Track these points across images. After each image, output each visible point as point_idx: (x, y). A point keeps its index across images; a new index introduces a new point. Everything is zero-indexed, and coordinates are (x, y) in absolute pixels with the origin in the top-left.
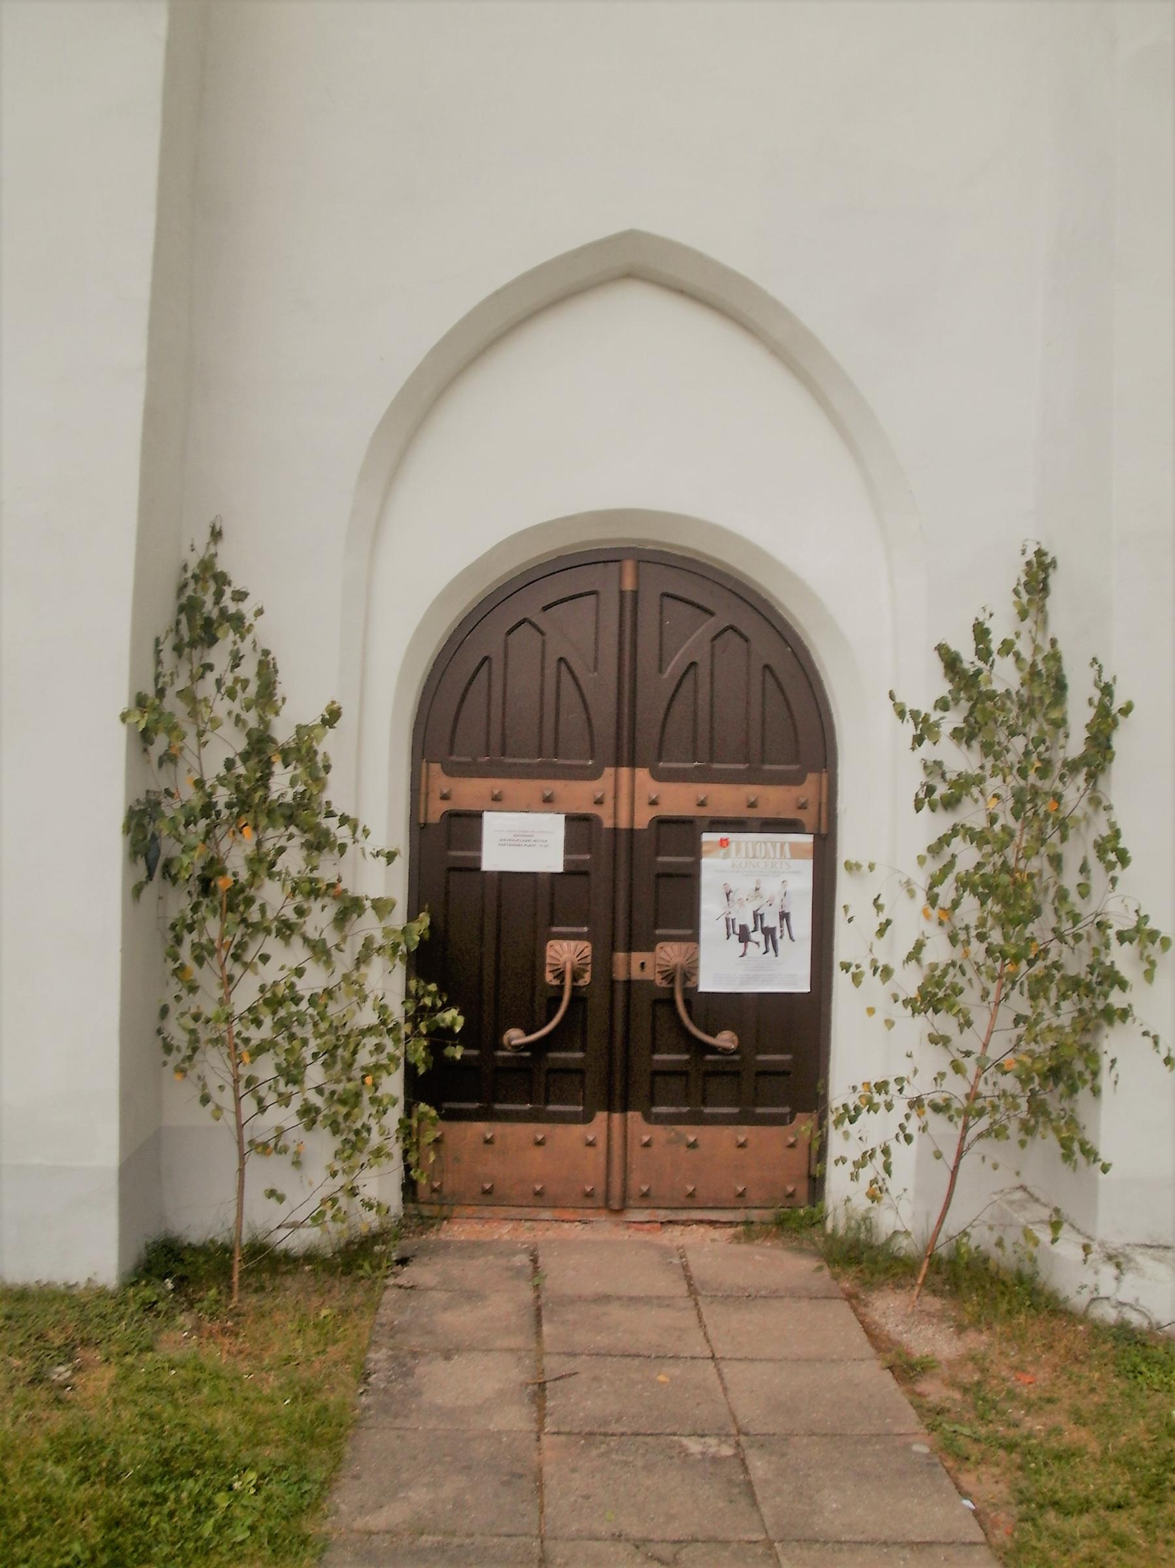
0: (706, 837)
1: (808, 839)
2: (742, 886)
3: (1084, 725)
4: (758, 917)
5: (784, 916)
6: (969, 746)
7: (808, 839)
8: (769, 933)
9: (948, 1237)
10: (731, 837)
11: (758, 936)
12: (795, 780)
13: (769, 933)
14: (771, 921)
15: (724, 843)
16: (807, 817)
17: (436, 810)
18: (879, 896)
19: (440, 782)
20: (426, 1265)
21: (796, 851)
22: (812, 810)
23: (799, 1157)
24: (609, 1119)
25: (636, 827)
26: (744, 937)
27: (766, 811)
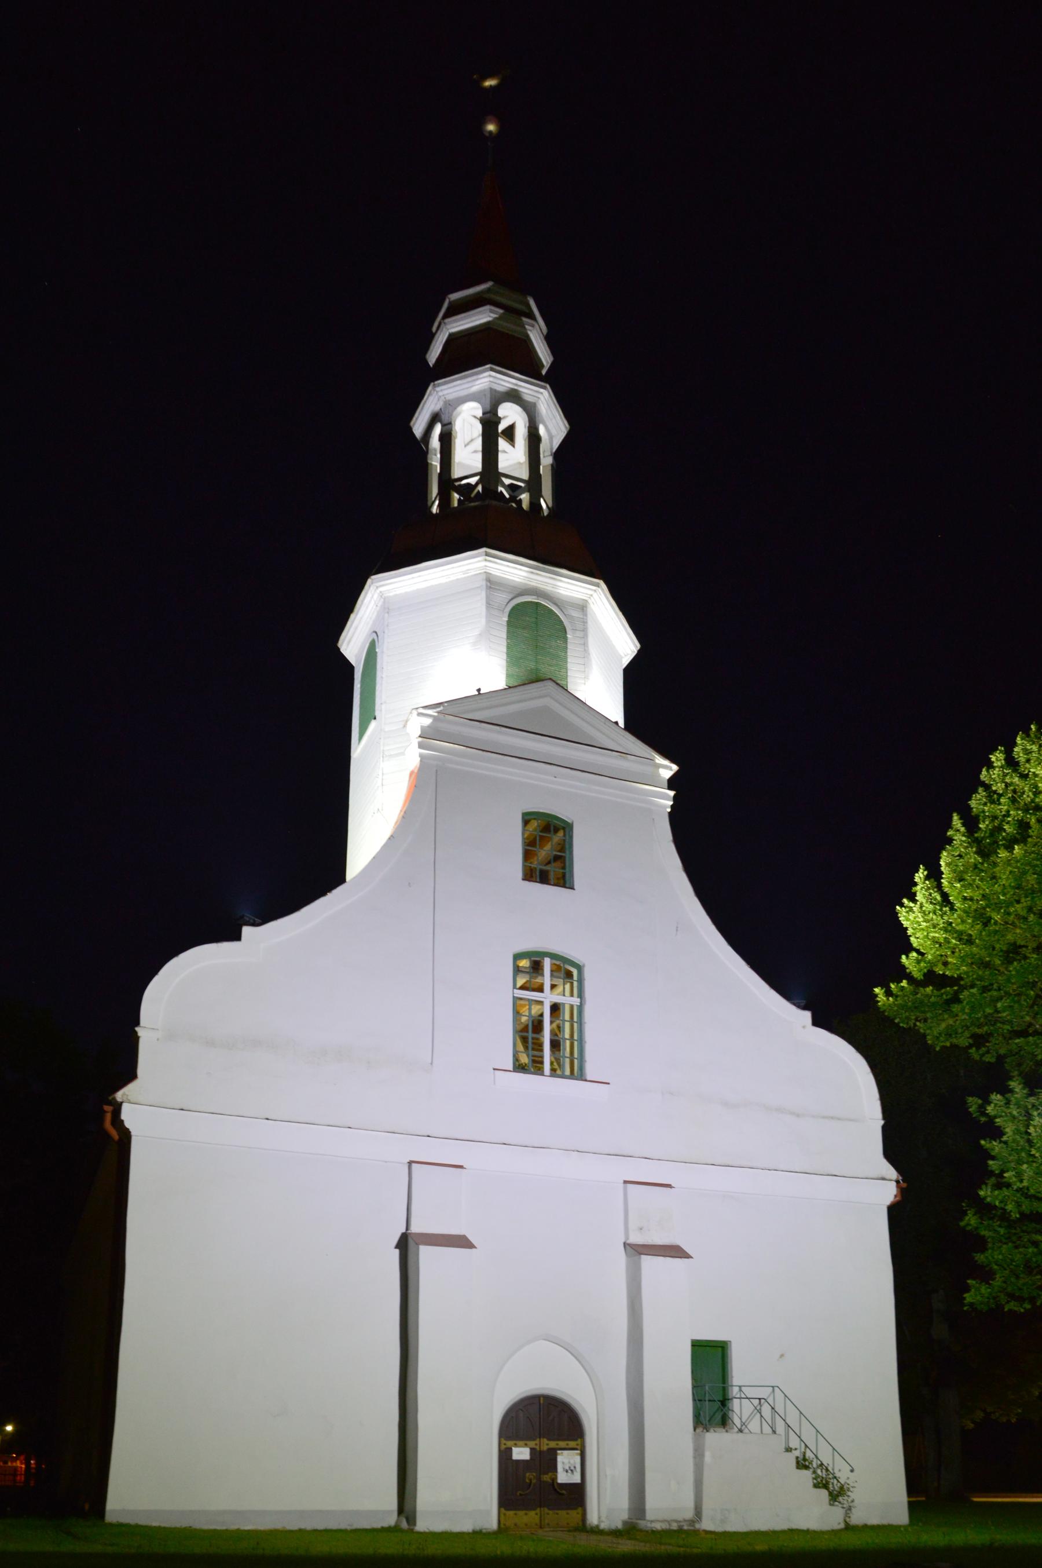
0: (559, 1452)
1: (579, 1452)
2: (566, 1461)
3: (586, 965)
4: (570, 1467)
5: (575, 1467)
6: (420, 736)
7: (579, 1452)
8: (572, 1470)
9: (557, 1524)
10: (563, 1451)
11: (570, 1471)
12: (576, 1440)
13: (572, 1470)
14: (572, 1468)
15: (562, 1453)
16: (579, 1447)
17: (503, 1447)
18: (462, 1242)
19: (503, 1441)
20: (655, 1528)
21: (577, 1454)
22: (580, 1446)
23: (580, 1516)
24: (540, 1510)
25: (542, 1449)
26: (567, 1471)
27: (570, 1446)
